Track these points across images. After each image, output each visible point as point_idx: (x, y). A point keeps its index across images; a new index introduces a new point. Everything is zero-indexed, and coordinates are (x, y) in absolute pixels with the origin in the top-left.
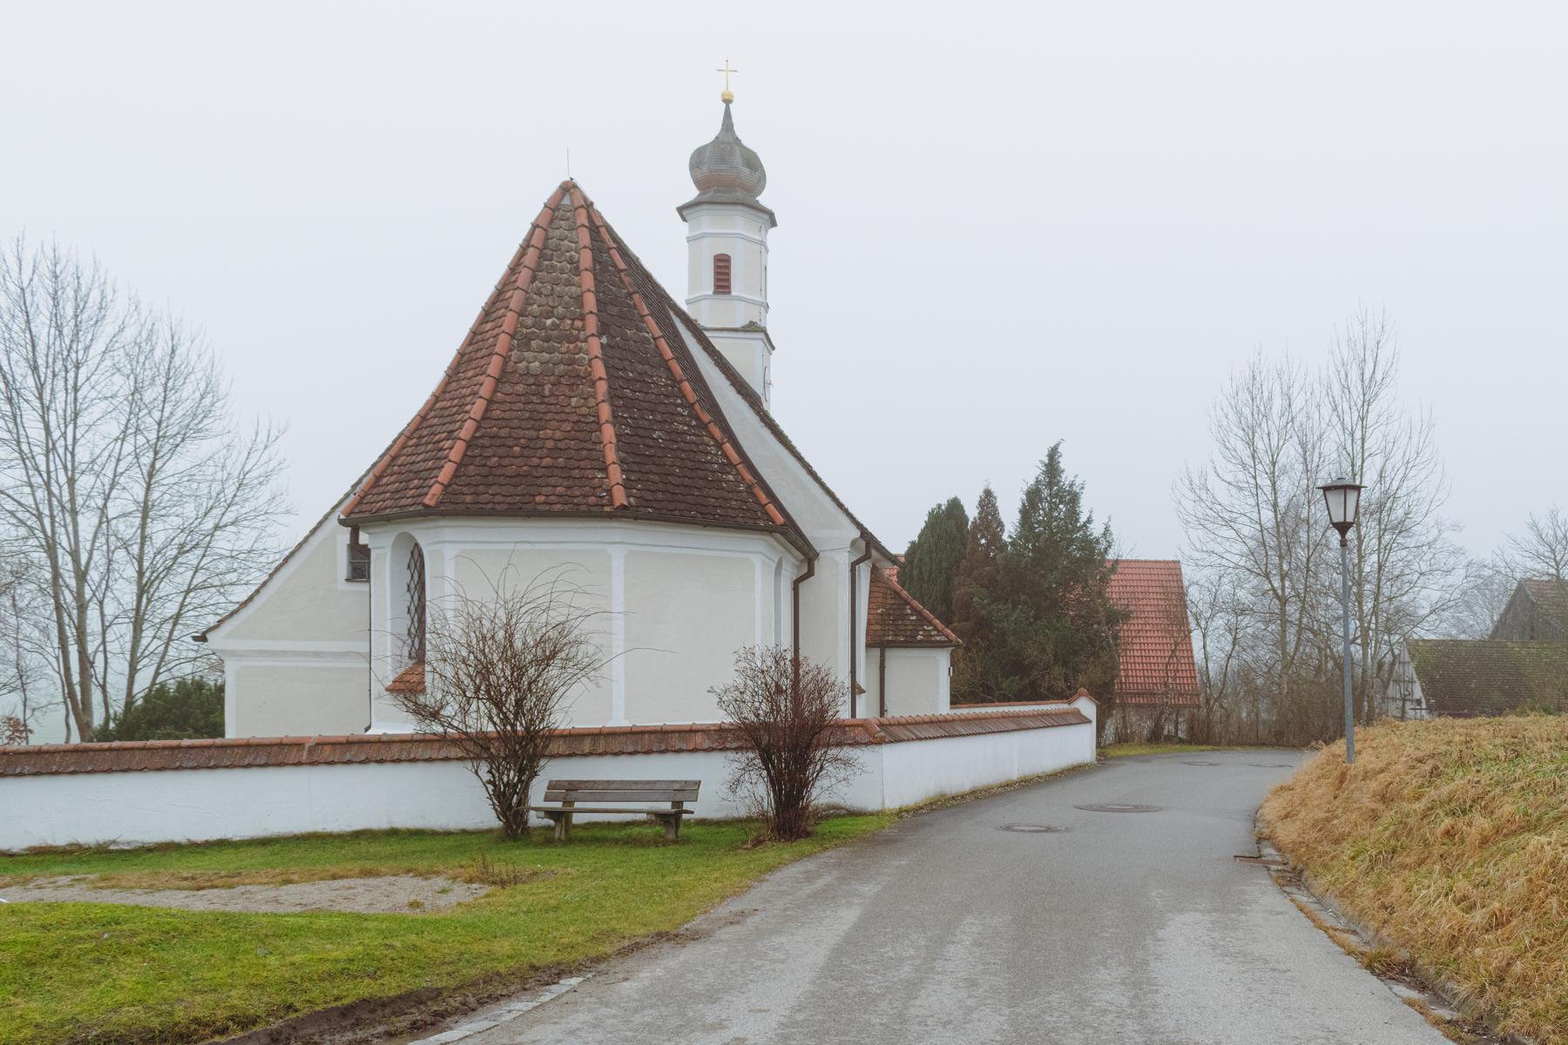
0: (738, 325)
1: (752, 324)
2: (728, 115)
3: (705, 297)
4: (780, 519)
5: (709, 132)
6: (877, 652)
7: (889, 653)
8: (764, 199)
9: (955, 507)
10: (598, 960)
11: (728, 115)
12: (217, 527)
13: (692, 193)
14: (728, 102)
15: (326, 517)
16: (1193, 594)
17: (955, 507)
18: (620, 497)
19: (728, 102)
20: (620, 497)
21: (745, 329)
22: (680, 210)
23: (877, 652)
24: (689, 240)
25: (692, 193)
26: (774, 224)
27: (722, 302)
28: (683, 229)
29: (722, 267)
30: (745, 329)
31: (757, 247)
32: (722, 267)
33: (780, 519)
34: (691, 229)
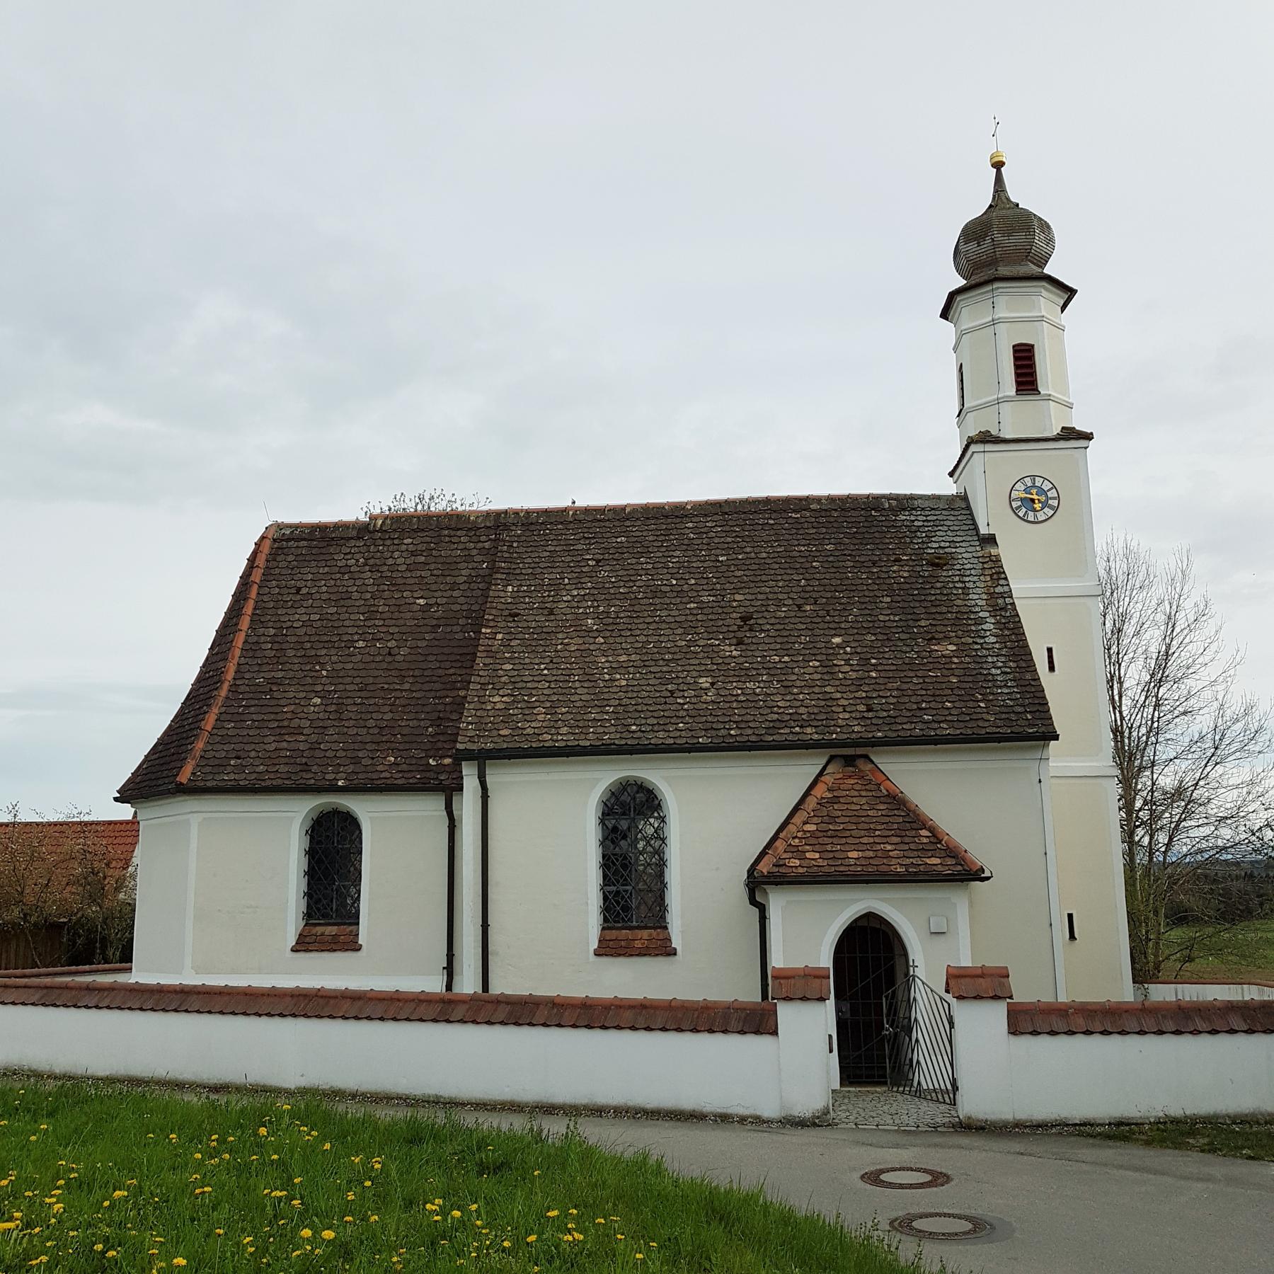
2: (999, 180)
3: (1008, 400)
11: (999, 180)
14: (998, 165)
19: (998, 165)
27: (1028, 405)
29: (1024, 358)
32: (1024, 358)
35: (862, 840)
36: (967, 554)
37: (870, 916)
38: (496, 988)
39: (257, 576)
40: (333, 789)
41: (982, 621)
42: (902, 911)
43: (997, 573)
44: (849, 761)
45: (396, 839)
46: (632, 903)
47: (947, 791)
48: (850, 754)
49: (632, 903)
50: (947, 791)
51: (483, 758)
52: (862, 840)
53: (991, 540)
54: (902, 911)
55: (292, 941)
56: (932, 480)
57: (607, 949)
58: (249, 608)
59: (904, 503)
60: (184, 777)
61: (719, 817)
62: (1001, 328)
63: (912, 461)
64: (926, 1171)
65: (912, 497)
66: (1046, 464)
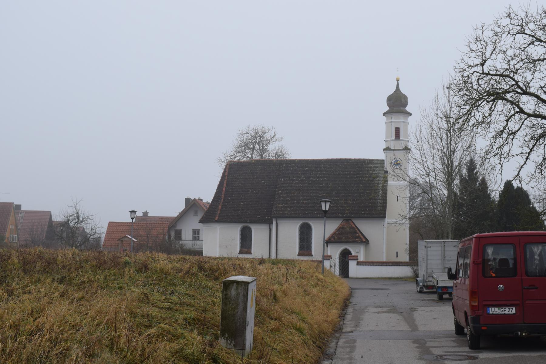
0: (401, 148)
2: (398, 84)
3: (393, 140)
4: (364, 240)
5: (391, 91)
8: (408, 109)
11: (398, 84)
13: (387, 108)
14: (398, 80)
15: (324, 248)
16: (531, 197)
19: (398, 80)
21: (403, 149)
24: (386, 123)
25: (387, 108)
26: (135, 212)
27: (397, 142)
29: (397, 130)
32: (397, 130)
33: (364, 240)
34: (387, 120)
35: (348, 236)
36: (382, 174)
37: (346, 249)
38: (280, 257)
39: (226, 174)
40: (247, 222)
41: (380, 192)
42: (353, 249)
43: (386, 181)
44: (347, 220)
45: (259, 234)
46: (305, 246)
47: (366, 227)
48: (348, 219)
49: (305, 246)
50: (366, 227)
51: (277, 218)
52: (348, 236)
53: (387, 172)
54: (353, 249)
55: (238, 252)
56: (379, 155)
57: (300, 254)
58: (225, 181)
59: (371, 161)
60: (216, 219)
61: (321, 230)
62: (393, 124)
63: (374, 152)
64: (324, 246)
65: (373, 160)
66: (400, 155)
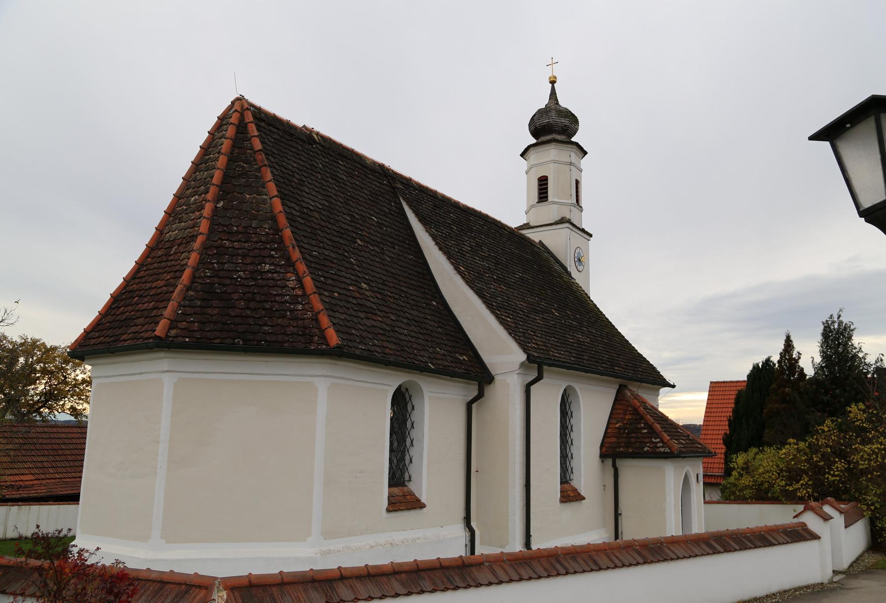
1: (563, 218)
2: (553, 89)
5: (542, 102)
6: (609, 462)
7: (619, 462)
9: (758, 365)
10: (371, 170)
11: (553, 89)
12: (143, 325)
14: (553, 83)
17: (758, 365)
18: (334, 338)
19: (553, 83)
20: (334, 338)
22: (522, 155)
23: (609, 462)
27: (544, 207)
28: (523, 164)
30: (556, 223)
31: (567, 168)
